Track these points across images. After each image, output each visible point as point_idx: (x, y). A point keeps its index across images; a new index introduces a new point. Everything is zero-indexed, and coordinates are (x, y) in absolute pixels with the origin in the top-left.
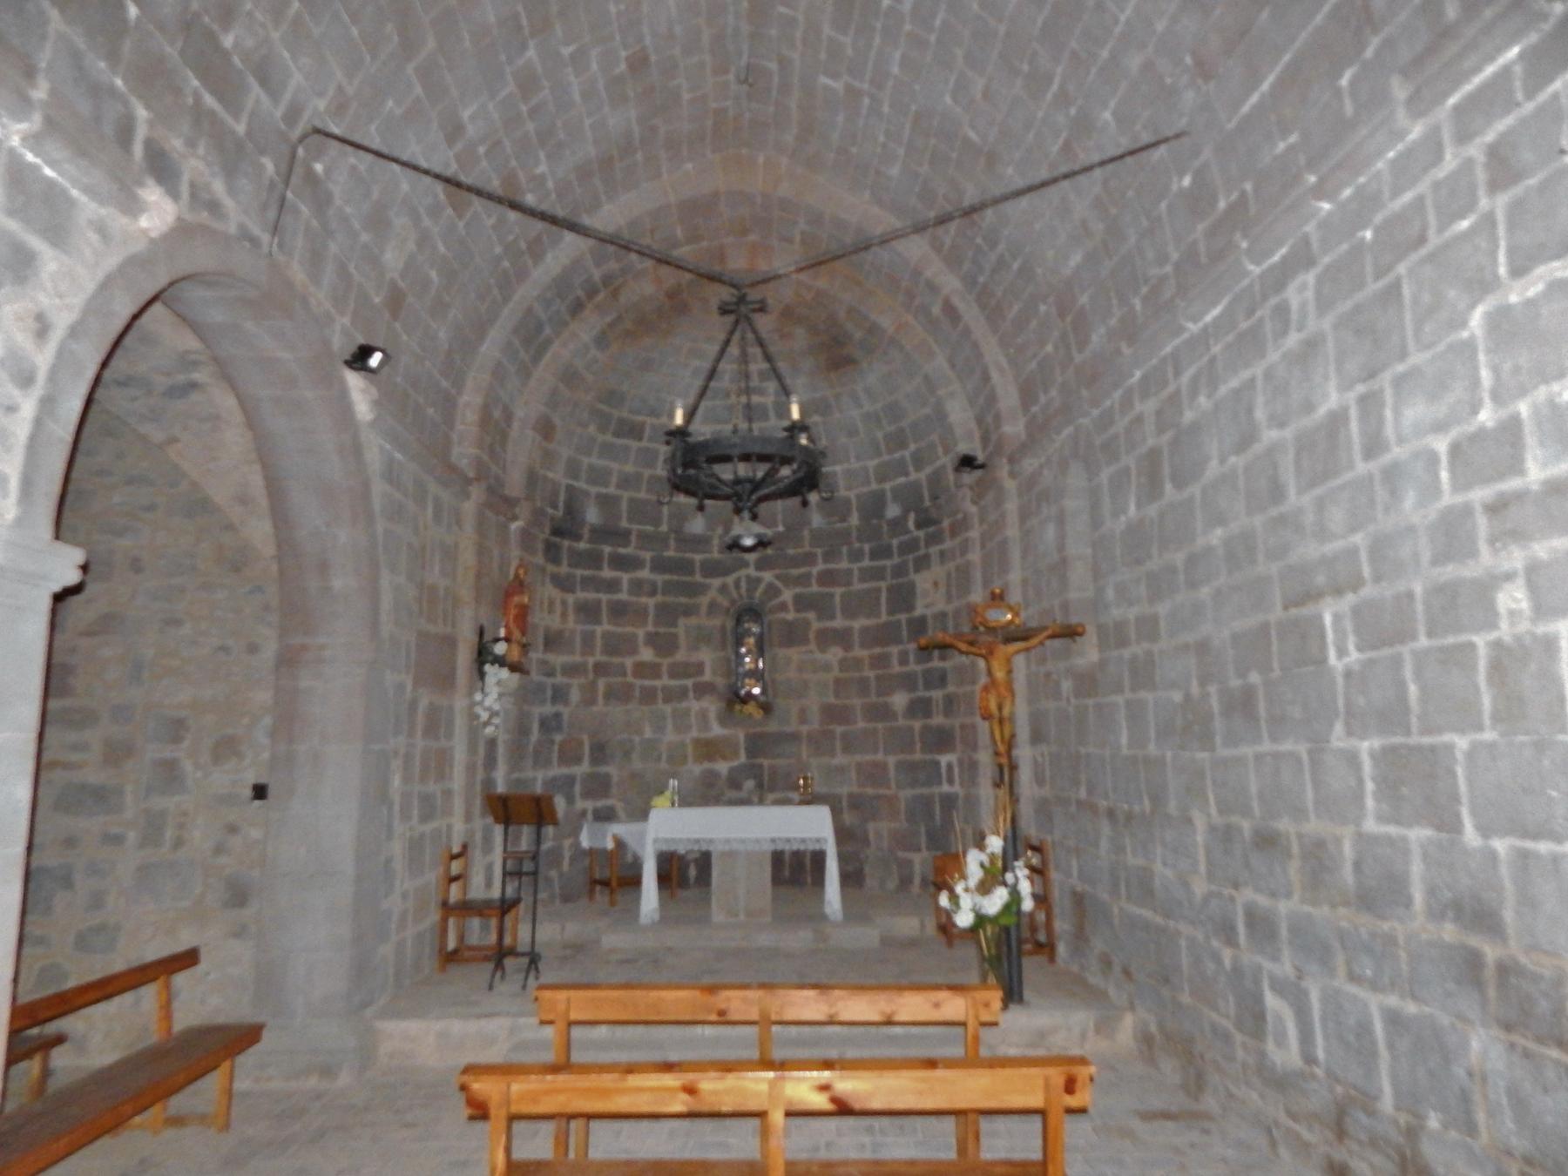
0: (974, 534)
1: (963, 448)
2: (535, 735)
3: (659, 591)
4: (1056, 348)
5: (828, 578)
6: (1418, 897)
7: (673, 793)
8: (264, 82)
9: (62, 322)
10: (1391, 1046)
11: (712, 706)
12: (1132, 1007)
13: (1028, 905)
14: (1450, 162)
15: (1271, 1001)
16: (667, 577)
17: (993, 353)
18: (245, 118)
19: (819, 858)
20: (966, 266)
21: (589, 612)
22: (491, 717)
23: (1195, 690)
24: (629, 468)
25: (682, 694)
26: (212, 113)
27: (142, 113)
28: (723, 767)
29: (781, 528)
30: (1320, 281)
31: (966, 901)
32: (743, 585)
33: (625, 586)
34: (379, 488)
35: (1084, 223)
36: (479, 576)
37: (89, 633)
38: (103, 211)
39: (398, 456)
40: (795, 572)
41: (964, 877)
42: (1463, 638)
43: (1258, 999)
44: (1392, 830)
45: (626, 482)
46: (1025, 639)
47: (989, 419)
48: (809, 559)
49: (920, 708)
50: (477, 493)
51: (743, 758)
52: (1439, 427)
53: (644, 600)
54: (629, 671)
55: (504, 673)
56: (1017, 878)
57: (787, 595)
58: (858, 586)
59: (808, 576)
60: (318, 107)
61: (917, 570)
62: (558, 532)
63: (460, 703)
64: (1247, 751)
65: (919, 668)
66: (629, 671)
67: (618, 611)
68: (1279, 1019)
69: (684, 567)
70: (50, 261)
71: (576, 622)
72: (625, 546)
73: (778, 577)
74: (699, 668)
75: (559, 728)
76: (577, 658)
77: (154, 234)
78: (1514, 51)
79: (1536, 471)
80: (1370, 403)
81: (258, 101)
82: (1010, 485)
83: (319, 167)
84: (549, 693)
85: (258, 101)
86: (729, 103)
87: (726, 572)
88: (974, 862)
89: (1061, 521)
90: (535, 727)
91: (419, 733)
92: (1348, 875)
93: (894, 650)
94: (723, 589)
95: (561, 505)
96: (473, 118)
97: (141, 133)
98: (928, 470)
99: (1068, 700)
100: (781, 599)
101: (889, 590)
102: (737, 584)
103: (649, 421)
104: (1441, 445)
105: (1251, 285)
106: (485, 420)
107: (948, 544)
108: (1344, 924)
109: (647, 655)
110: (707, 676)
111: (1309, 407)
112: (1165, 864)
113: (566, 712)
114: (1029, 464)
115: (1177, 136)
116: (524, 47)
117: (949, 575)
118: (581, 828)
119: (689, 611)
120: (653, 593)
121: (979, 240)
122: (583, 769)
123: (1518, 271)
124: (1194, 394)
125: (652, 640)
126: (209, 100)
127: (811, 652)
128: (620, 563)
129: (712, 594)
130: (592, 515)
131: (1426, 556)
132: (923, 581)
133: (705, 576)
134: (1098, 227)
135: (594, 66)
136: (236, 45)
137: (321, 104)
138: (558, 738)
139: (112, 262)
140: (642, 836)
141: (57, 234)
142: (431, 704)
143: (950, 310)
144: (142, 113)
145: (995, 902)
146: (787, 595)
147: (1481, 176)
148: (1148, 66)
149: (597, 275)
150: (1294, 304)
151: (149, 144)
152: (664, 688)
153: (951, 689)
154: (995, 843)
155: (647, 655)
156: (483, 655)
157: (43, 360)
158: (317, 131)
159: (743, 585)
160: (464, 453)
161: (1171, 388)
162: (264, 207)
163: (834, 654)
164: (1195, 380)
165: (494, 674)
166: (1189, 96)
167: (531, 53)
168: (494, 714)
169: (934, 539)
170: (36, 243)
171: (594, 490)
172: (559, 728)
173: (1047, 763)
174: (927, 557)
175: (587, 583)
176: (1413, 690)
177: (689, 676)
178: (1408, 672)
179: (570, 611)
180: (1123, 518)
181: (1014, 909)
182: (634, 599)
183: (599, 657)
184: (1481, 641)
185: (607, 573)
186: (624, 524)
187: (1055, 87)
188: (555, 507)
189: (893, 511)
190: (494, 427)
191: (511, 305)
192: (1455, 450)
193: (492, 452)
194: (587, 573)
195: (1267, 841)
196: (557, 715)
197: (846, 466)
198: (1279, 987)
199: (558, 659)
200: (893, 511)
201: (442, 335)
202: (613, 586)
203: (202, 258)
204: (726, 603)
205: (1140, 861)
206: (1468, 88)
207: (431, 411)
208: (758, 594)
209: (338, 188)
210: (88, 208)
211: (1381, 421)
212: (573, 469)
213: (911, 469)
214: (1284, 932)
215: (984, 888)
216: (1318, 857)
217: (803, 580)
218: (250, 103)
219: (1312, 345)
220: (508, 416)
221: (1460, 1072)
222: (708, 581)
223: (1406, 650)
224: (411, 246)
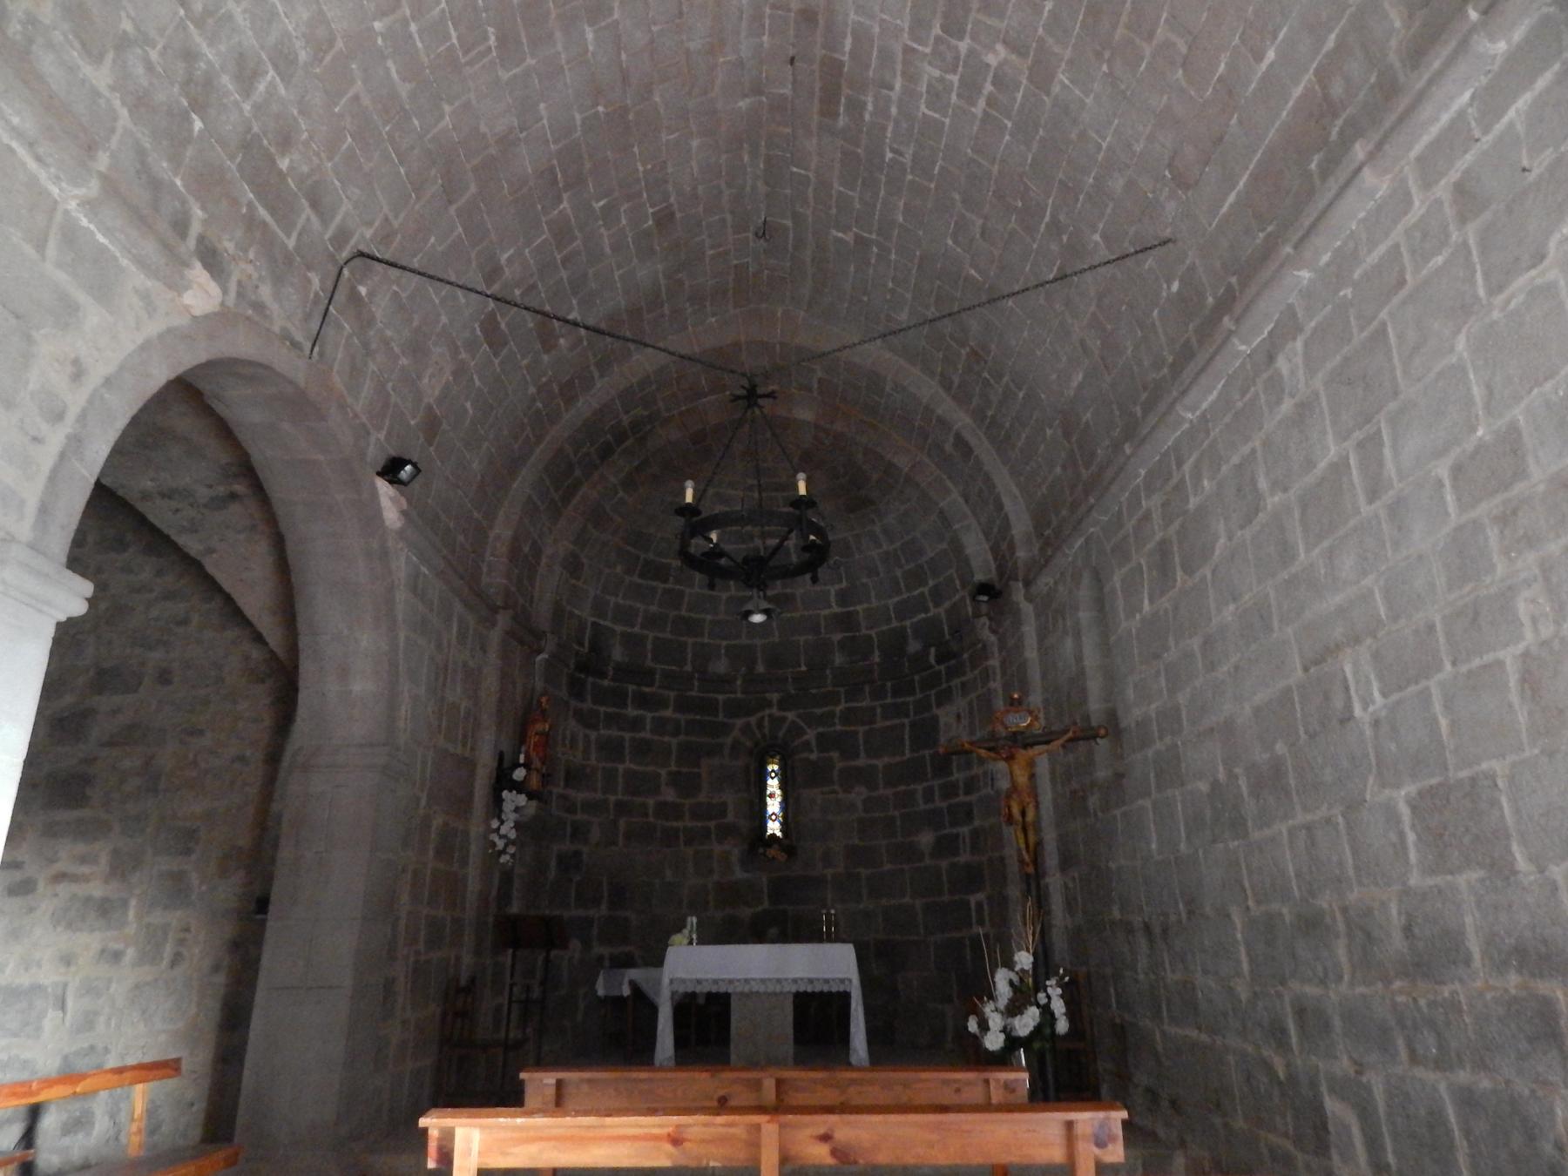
0: (994, 662)
1: (979, 577)
2: (552, 873)
4: (1064, 467)
5: (847, 717)
6: (1474, 946)
7: (691, 932)
8: (315, 204)
9: (98, 373)
10: (1467, 1133)
11: (735, 850)
12: (1183, 1144)
13: (1062, 1026)
14: (1418, 209)
15: (1332, 1105)
16: (690, 716)
17: (1005, 483)
18: (294, 235)
19: (845, 997)
20: (975, 401)
21: (612, 750)
22: (506, 845)
23: (1222, 776)
26: (265, 224)
27: (198, 213)
28: (746, 912)
29: (804, 668)
30: (1306, 345)
31: (996, 1021)
32: (766, 723)
34: (402, 596)
35: (1082, 343)
36: (501, 701)
37: (111, 743)
38: (149, 283)
39: (424, 569)
40: (818, 711)
41: (992, 997)
42: (1489, 658)
43: (1319, 1109)
44: (1439, 880)
45: (652, 621)
46: (1047, 743)
47: (1004, 546)
49: (947, 846)
50: (503, 620)
51: (766, 905)
52: (1439, 454)
53: (666, 739)
54: (651, 811)
55: (522, 800)
56: (1049, 997)
57: (810, 735)
58: (880, 724)
59: (832, 714)
60: (364, 237)
61: (939, 705)
62: (583, 667)
63: (476, 830)
64: (1282, 828)
65: (944, 805)
66: (651, 811)
67: (643, 750)
68: (1347, 1128)
70: (93, 316)
73: (799, 716)
74: (722, 810)
76: (599, 796)
77: (197, 312)
78: (1467, 95)
79: (1539, 472)
80: (1370, 447)
81: (308, 219)
82: (1027, 609)
83: (363, 290)
85: (308, 219)
86: (749, 260)
88: (1002, 981)
89: (1077, 635)
91: (431, 853)
92: (1398, 942)
93: (919, 788)
94: (746, 729)
95: (587, 644)
96: (509, 260)
97: (195, 229)
98: (947, 604)
99: (1096, 815)
100: (806, 737)
101: (913, 725)
102: (760, 725)
104: (1442, 470)
105: (1243, 365)
106: (514, 553)
107: (969, 676)
108: (1400, 999)
109: (669, 795)
110: (730, 817)
111: (1310, 464)
112: (1205, 972)
114: (1044, 582)
115: (1165, 243)
116: (559, 200)
117: (970, 703)
118: (598, 975)
120: (676, 733)
121: (986, 375)
123: (1495, 289)
124: (1197, 476)
125: (675, 780)
126: (263, 213)
127: (834, 792)
128: (644, 701)
129: (736, 733)
130: (618, 654)
131: (1441, 581)
132: (945, 715)
134: (1095, 344)
135: (624, 222)
136: (291, 168)
137: (368, 233)
139: (153, 328)
140: (659, 982)
141: (103, 291)
142: (446, 824)
143: (961, 442)
144: (198, 213)
145: (1026, 1023)
146: (810, 735)
147: (1449, 211)
148: (1131, 184)
149: (626, 420)
150: (1285, 371)
151: (201, 239)
153: (977, 823)
154: (1024, 959)
155: (669, 795)
156: (502, 780)
157: (76, 401)
158: (361, 254)
159: (766, 723)
160: (495, 579)
161: (1175, 480)
162: (307, 317)
163: (859, 794)
164: (1197, 467)
165: (512, 800)
166: (1171, 207)
167: (565, 205)
168: (509, 842)
169: (953, 673)
170: (81, 297)
171: (619, 628)
173: (1078, 888)
174: (949, 689)
176: (1444, 723)
178: (1437, 707)
179: (593, 746)
180: (1138, 616)
181: (1048, 1031)
182: (656, 738)
184: (1509, 656)
185: (632, 712)
186: (649, 663)
187: (1047, 219)
188: (581, 644)
189: (914, 646)
190: (524, 559)
191: (542, 446)
192: (1457, 470)
194: (611, 710)
195: (1312, 924)
196: (577, 854)
197: (865, 606)
198: (1342, 1089)
199: (580, 796)
200: (914, 646)
201: (475, 465)
202: (636, 724)
203: (242, 345)
204: (749, 744)
205: (1178, 976)
206: (1426, 139)
207: (461, 538)
208: (781, 734)
209: (381, 309)
210: (138, 279)
211: (1381, 464)
212: (599, 608)
213: (931, 605)
214: (1337, 1023)
215: (1014, 1009)
216: (1364, 931)
218: (301, 222)
219: (1305, 409)
220: (537, 551)
221: (1548, 1148)
222: (731, 721)
223: (1433, 684)
224: (448, 376)
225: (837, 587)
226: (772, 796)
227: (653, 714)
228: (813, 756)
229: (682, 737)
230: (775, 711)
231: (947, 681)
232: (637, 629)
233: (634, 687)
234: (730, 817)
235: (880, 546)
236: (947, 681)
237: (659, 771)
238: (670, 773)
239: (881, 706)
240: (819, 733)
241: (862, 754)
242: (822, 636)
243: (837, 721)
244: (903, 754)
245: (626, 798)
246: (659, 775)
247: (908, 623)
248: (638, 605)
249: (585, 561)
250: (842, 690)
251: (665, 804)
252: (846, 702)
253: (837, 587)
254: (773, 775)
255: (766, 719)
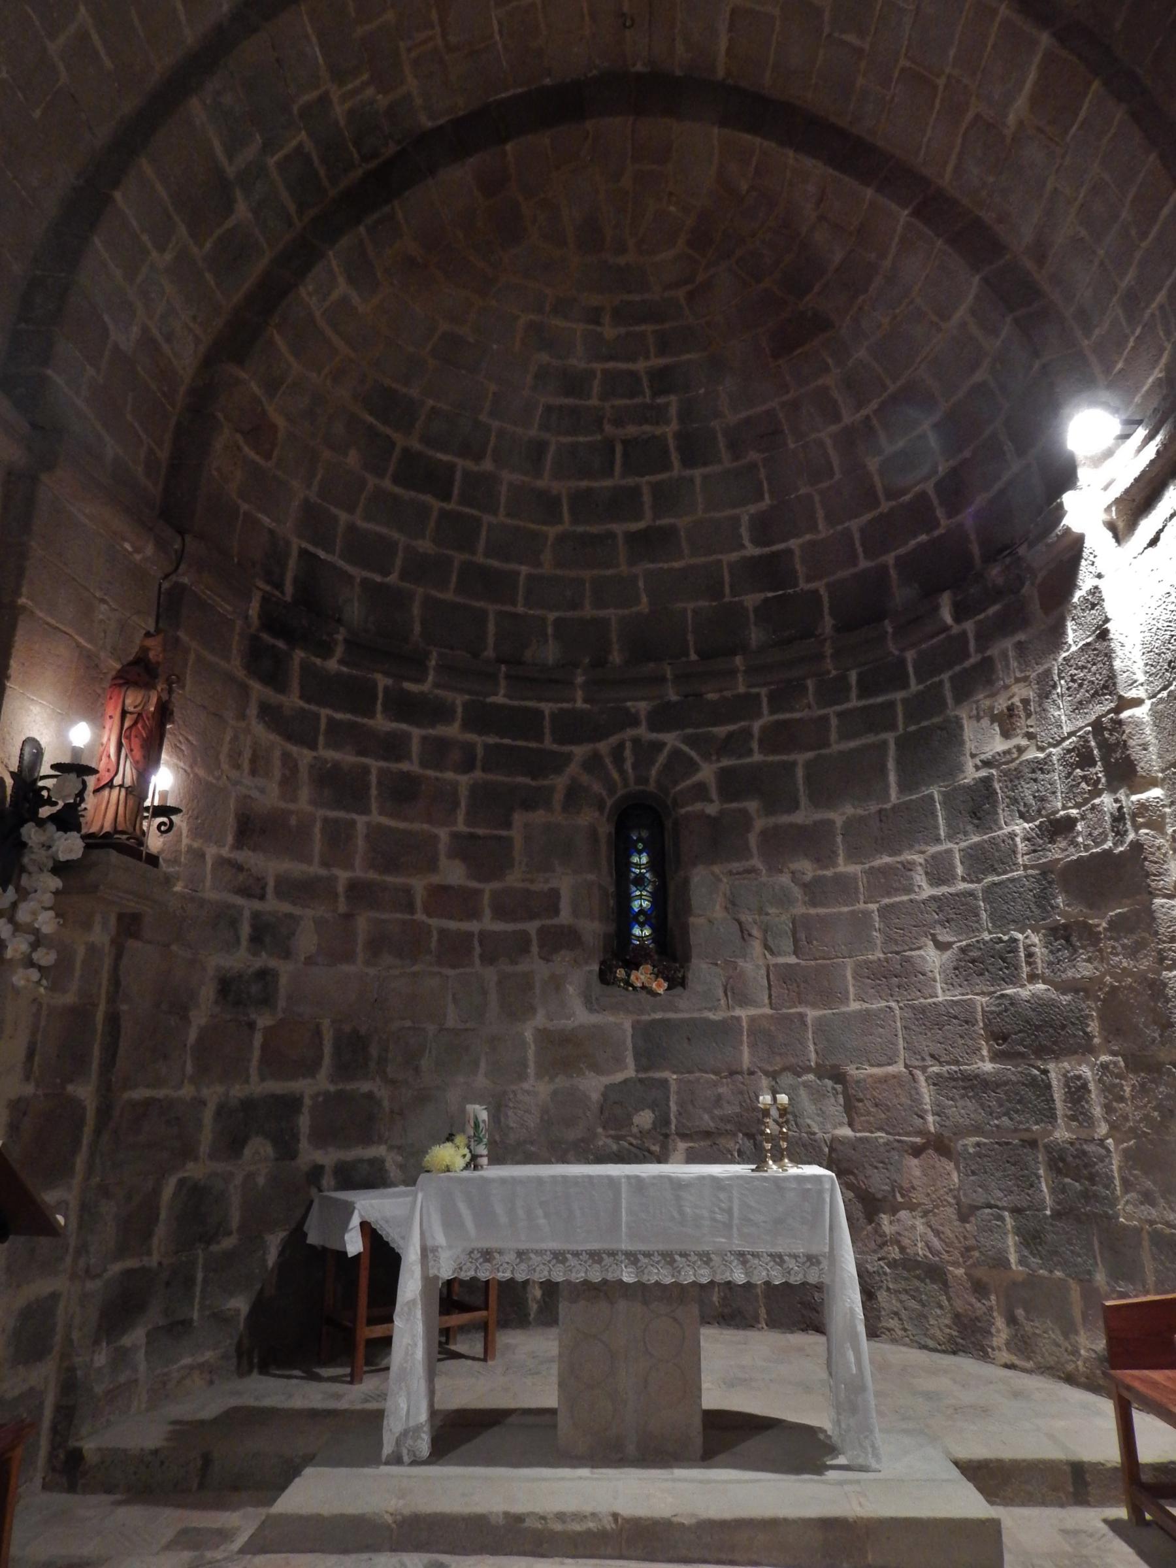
3: (479, 764)
16: (492, 740)
24: (425, 545)
25: (522, 945)
28: (593, 1085)
33: (415, 747)
40: (721, 731)
48: (747, 706)
51: (630, 1072)
53: (449, 775)
57: (707, 772)
62: (273, 622)
66: (419, 903)
69: (528, 724)
71: (313, 802)
72: (420, 680)
73: (687, 740)
75: (267, 1001)
76: (315, 869)
84: (245, 930)
87: (598, 734)
90: (208, 993)
94: (593, 764)
95: (289, 588)
102: (617, 754)
103: (462, 464)
109: (454, 873)
110: (565, 917)
113: (285, 970)
119: (531, 801)
120: (468, 765)
122: (321, 1083)
125: (464, 848)
129: (573, 768)
133: (562, 742)
138: (264, 1021)
146: (707, 772)
152: (483, 936)
155: (454, 873)
172: (267, 1001)
175: (338, 734)
177: (532, 916)
183: (360, 871)
185: (381, 723)
196: (264, 975)
202: (393, 747)
213: (940, 513)
217: (734, 744)
222: (566, 749)
225: (752, 509)
226: (639, 881)
227: (423, 732)
228: (712, 809)
229: (478, 774)
230: (642, 731)
231: (981, 648)
232: (392, 579)
233: (389, 682)
234: (565, 917)
235: (837, 418)
236: (981, 648)
237: (435, 830)
238: (455, 836)
239: (840, 715)
240: (723, 769)
241: (804, 801)
242: (727, 599)
243: (755, 746)
244: (886, 797)
245: (372, 875)
246: (436, 837)
247: (890, 559)
248: (396, 535)
249: (280, 422)
250: (763, 691)
251: (444, 889)
252: (772, 712)
253: (752, 509)
254: (640, 846)
255: (628, 744)
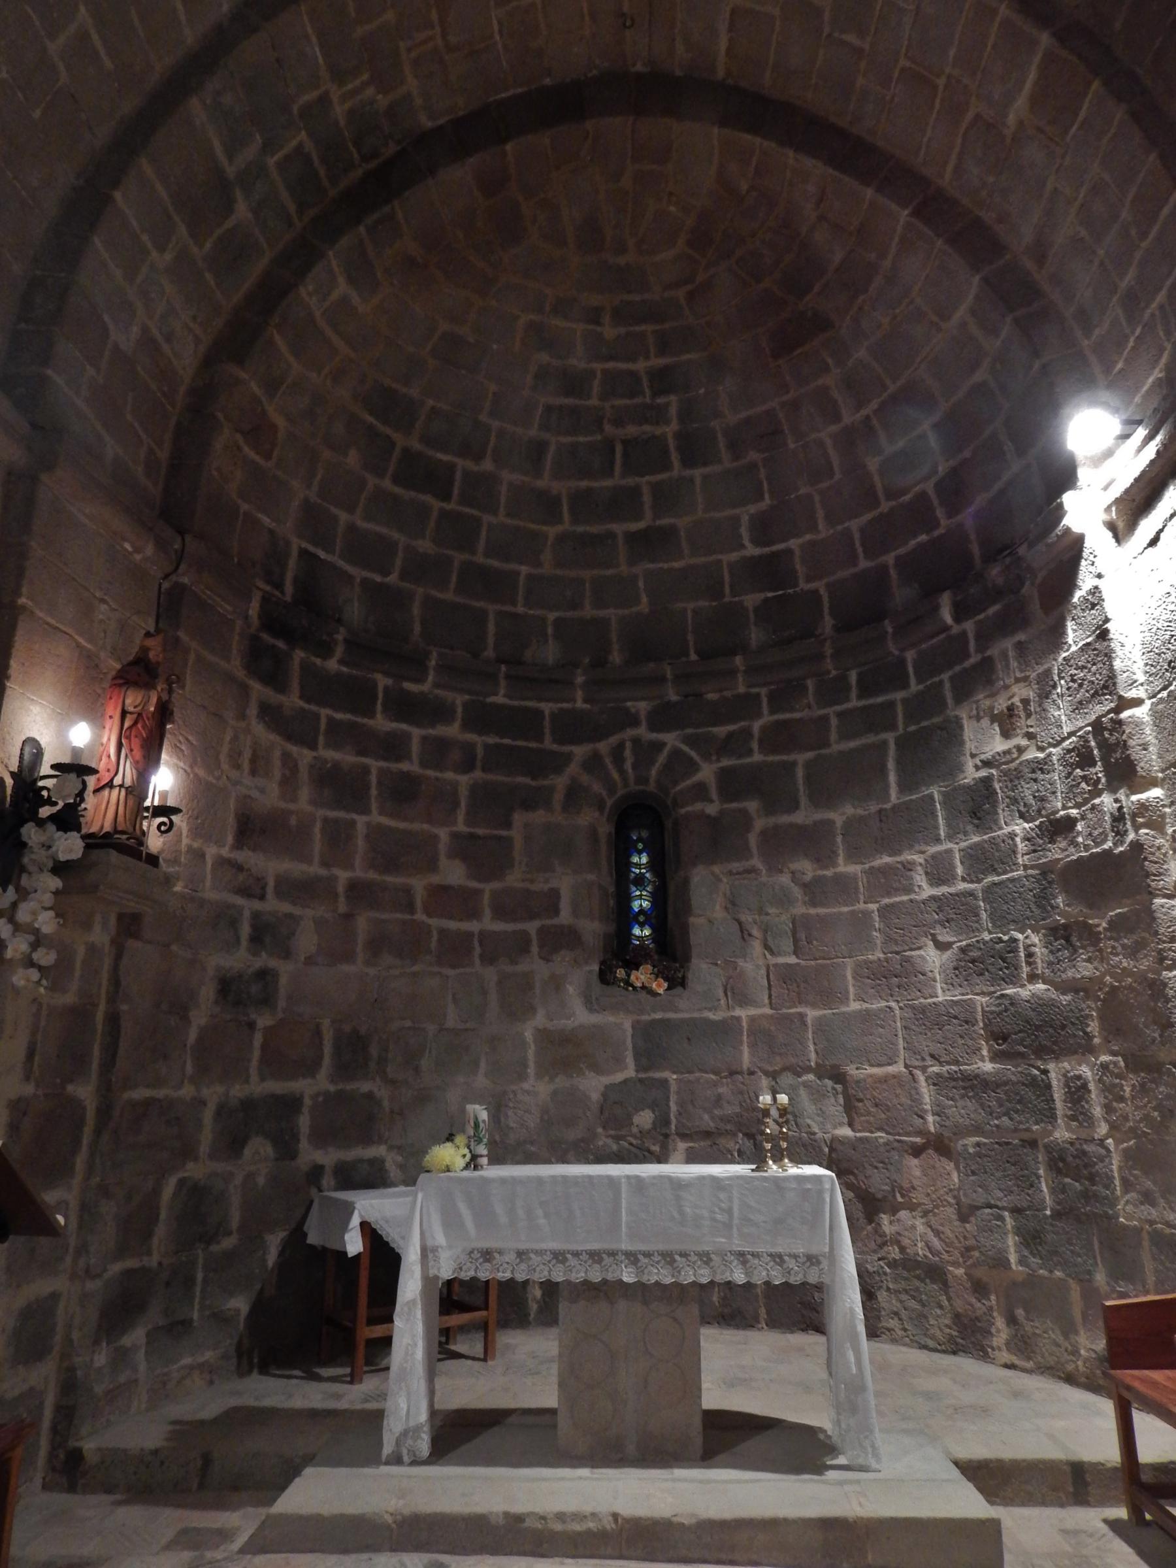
3: (479, 764)
16: (492, 740)
24: (425, 545)
25: (522, 945)
28: (593, 1085)
33: (415, 747)
40: (721, 731)
48: (747, 706)
51: (630, 1072)
53: (449, 775)
57: (707, 772)
62: (273, 622)
66: (419, 903)
69: (528, 724)
71: (313, 802)
72: (420, 680)
73: (687, 740)
75: (267, 1001)
76: (315, 869)
84: (245, 930)
87: (598, 734)
90: (208, 993)
94: (593, 764)
95: (289, 588)
102: (617, 754)
103: (462, 464)
109: (454, 873)
110: (565, 917)
113: (285, 970)
119: (531, 801)
120: (468, 765)
122: (321, 1083)
125: (464, 848)
129: (573, 768)
133: (562, 742)
138: (264, 1021)
146: (707, 772)
152: (483, 936)
155: (454, 873)
172: (267, 1001)
175: (338, 734)
177: (532, 916)
183: (360, 871)
185: (381, 723)
193: (682, 1107)
196: (264, 975)
202: (393, 747)
213: (940, 513)
217: (734, 744)
222: (566, 749)
225: (752, 509)
226: (639, 881)
227: (423, 732)
228: (712, 809)
229: (478, 774)
230: (642, 731)
231: (981, 648)
232: (392, 579)
233: (389, 682)
234: (565, 917)
235: (837, 418)
236: (981, 648)
237: (435, 830)
238: (455, 836)
239: (840, 715)
240: (723, 769)
241: (804, 801)
242: (727, 599)
243: (755, 746)
244: (886, 797)
245: (372, 875)
246: (436, 837)
247: (890, 559)
248: (396, 535)
249: (280, 422)
250: (763, 691)
251: (444, 889)
252: (772, 712)
253: (752, 509)
254: (640, 846)
255: (628, 744)
